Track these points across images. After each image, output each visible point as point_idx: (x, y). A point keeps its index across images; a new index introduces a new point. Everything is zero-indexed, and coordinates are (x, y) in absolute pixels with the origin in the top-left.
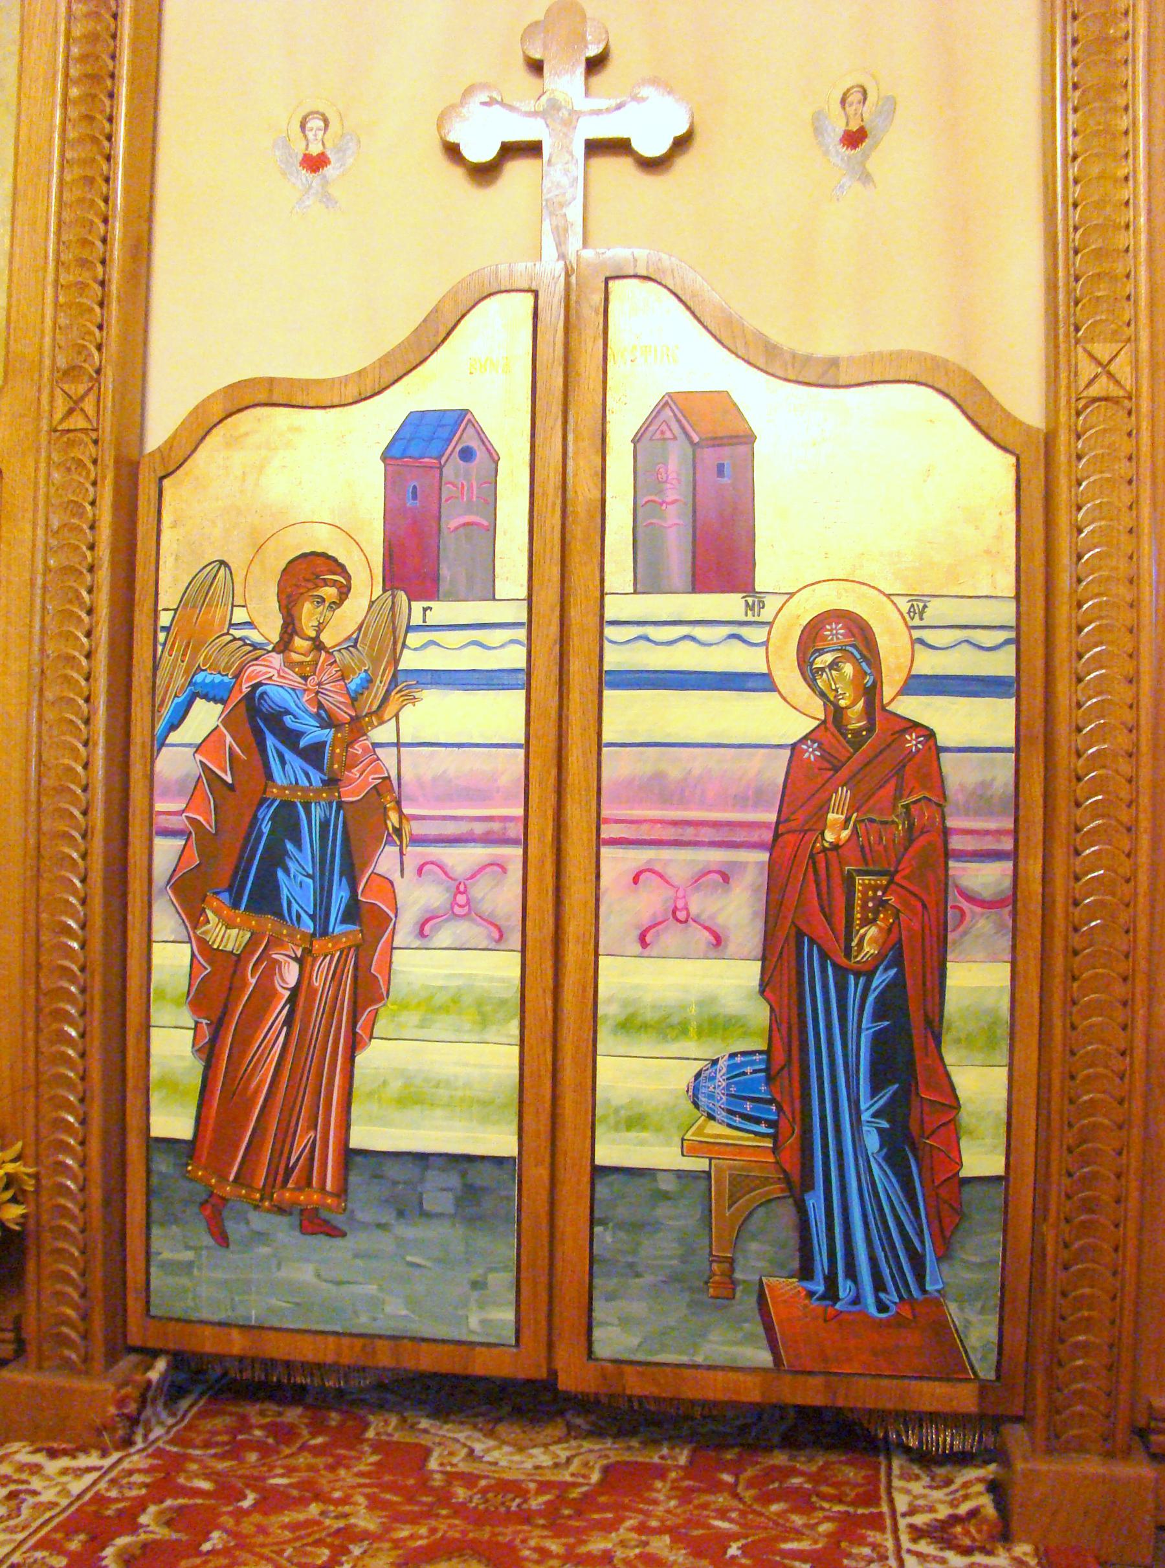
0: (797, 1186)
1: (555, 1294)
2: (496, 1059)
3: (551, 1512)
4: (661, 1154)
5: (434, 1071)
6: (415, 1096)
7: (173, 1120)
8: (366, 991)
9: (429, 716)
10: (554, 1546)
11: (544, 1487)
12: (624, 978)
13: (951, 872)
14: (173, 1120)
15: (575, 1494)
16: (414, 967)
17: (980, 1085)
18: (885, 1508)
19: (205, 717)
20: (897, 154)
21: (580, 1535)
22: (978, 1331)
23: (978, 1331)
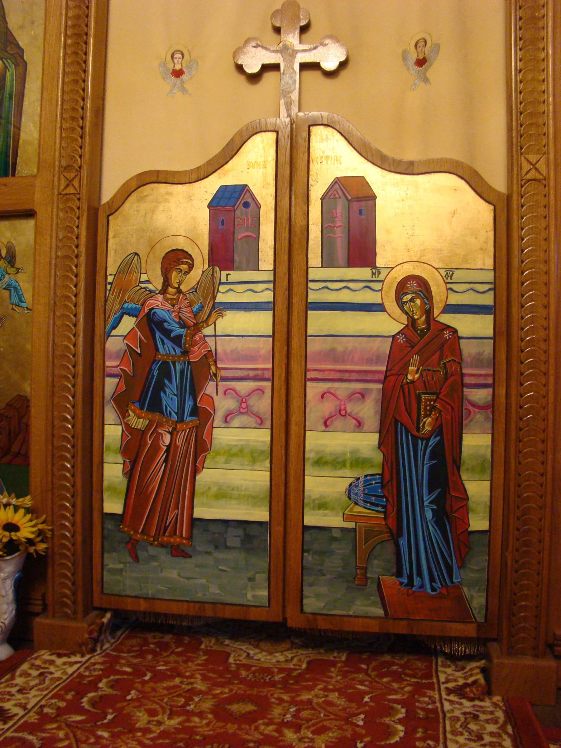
0: (395, 535)
1: (286, 584)
2: (259, 477)
3: (284, 682)
4: (334, 521)
5: (232, 483)
6: (223, 494)
7: (113, 505)
8: (201, 447)
9: (230, 322)
10: (286, 697)
11: (281, 670)
12: (317, 441)
13: (465, 393)
14: (113, 505)
15: (295, 673)
16: (223, 436)
17: (478, 489)
18: (435, 680)
19: (128, 324)
20: (442, 70)
21: (297, 692)
22: (477, 600)
23: (477, 600)
